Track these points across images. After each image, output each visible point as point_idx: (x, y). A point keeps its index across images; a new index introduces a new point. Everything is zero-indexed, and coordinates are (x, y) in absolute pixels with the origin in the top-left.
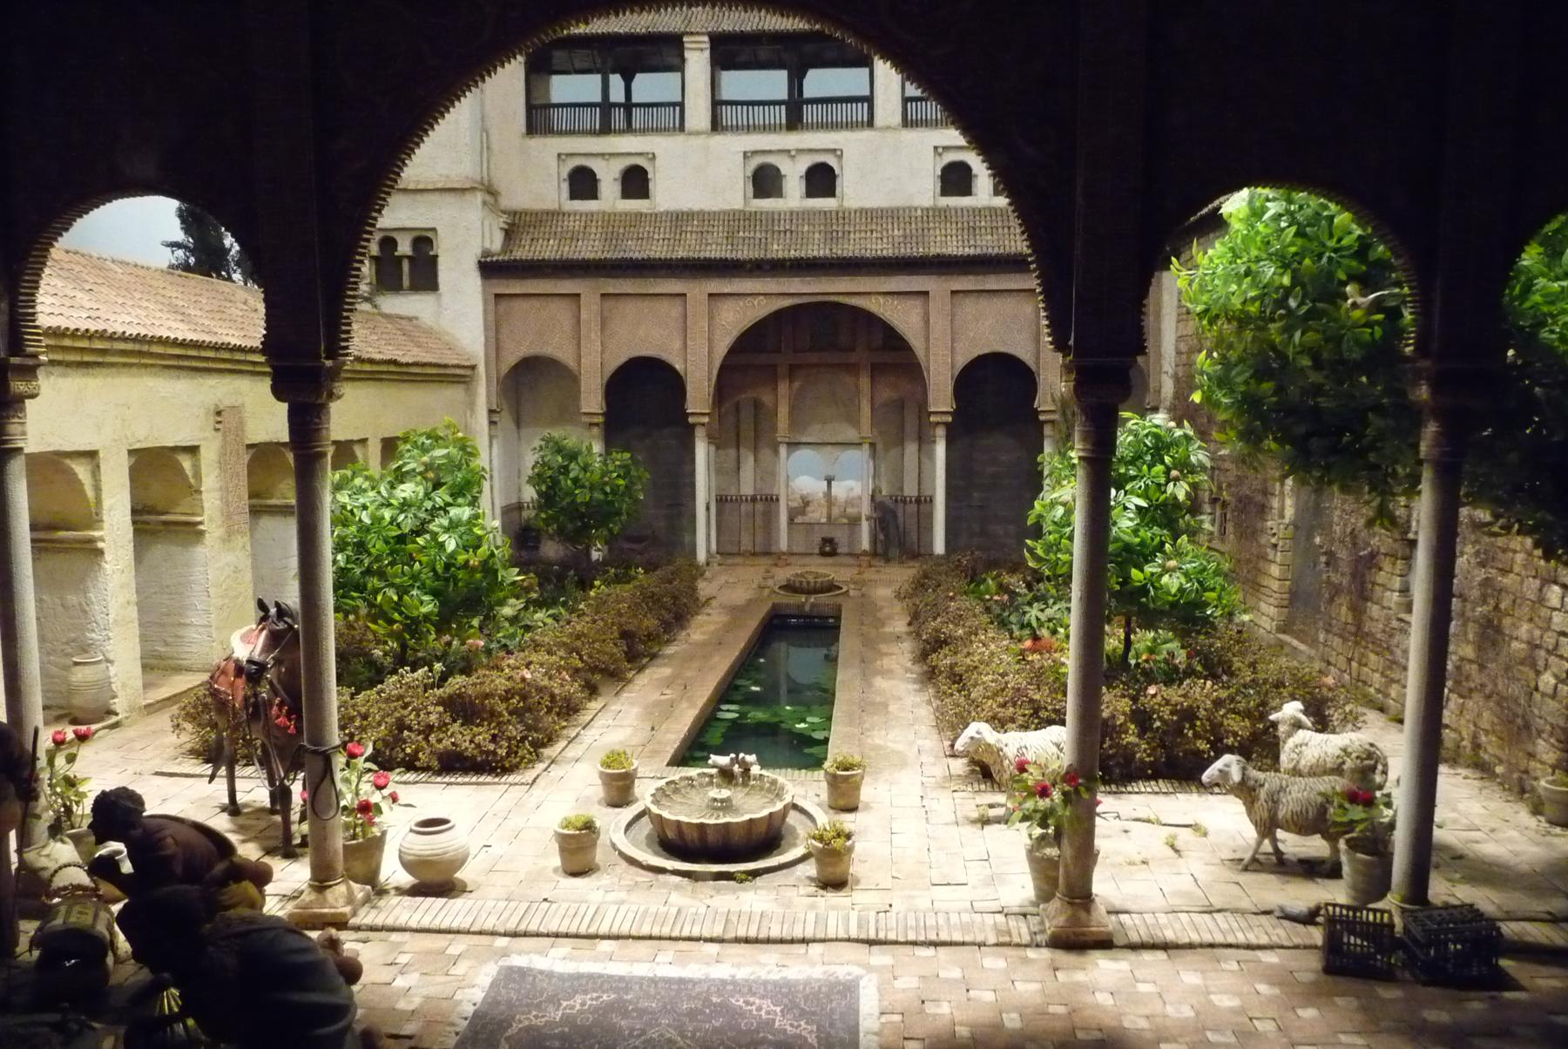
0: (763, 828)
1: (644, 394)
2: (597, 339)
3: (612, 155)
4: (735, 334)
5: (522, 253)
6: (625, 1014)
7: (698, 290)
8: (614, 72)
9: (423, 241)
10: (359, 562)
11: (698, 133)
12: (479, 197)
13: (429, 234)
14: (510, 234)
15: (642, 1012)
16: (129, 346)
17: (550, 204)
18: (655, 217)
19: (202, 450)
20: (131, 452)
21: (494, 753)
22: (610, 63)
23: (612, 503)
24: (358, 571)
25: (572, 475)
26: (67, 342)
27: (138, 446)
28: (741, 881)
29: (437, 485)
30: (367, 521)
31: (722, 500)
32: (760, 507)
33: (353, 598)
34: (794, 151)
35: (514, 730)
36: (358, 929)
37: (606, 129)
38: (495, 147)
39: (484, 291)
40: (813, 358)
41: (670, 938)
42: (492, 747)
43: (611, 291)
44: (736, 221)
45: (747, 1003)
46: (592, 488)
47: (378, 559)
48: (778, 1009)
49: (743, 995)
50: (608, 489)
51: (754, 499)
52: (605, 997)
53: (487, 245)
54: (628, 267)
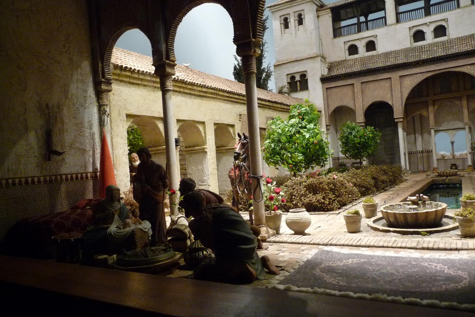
0: (433, 217)
1: (379, 113)
2: (360, 98)
3: (361, 38)
4: (410, 89)
5: (334, 73)
6: (371, 265)
7: (395, 76)
8: (361, 16)
9: (303, 76)
10: (278, 146)
11: (392, 25)
12: (319, 58)
13: (305, 73)
14: (330, 69)
15: (378, 265)
16: (213, 91)
17: (343, 58)
18: (378, 55)
19: (235, 126)
20: (215, 124)
21: (324, 203)
22: (359, 12)
23: (368, 143)
24: (278, 148)
25: (353, 134)
26: (195, 88)
27: (216, 122)
28: (424, 235)
29: (303, 119)
30: (281, 132)
31: (410, 153)
32: (425, 154)
33: (277, 158)
34: (428, 24)
35: (331, 196)
36: (270, 242)
37: (359, 31)
38: (324, 44)
39: (323, 88)
40: (443, 96)
41: (392, 247)
42: (323, 201)
43: (364, 81)
44: (406, 51)
45: (430, 265)
46: (360, 137)
47: (284, 144)
48: (446, 267)
49: (427, 262)
50: (366, 138)
51: (422, 152)
52: (362, 260)
53: (323, 73)
54: (370, 72)
